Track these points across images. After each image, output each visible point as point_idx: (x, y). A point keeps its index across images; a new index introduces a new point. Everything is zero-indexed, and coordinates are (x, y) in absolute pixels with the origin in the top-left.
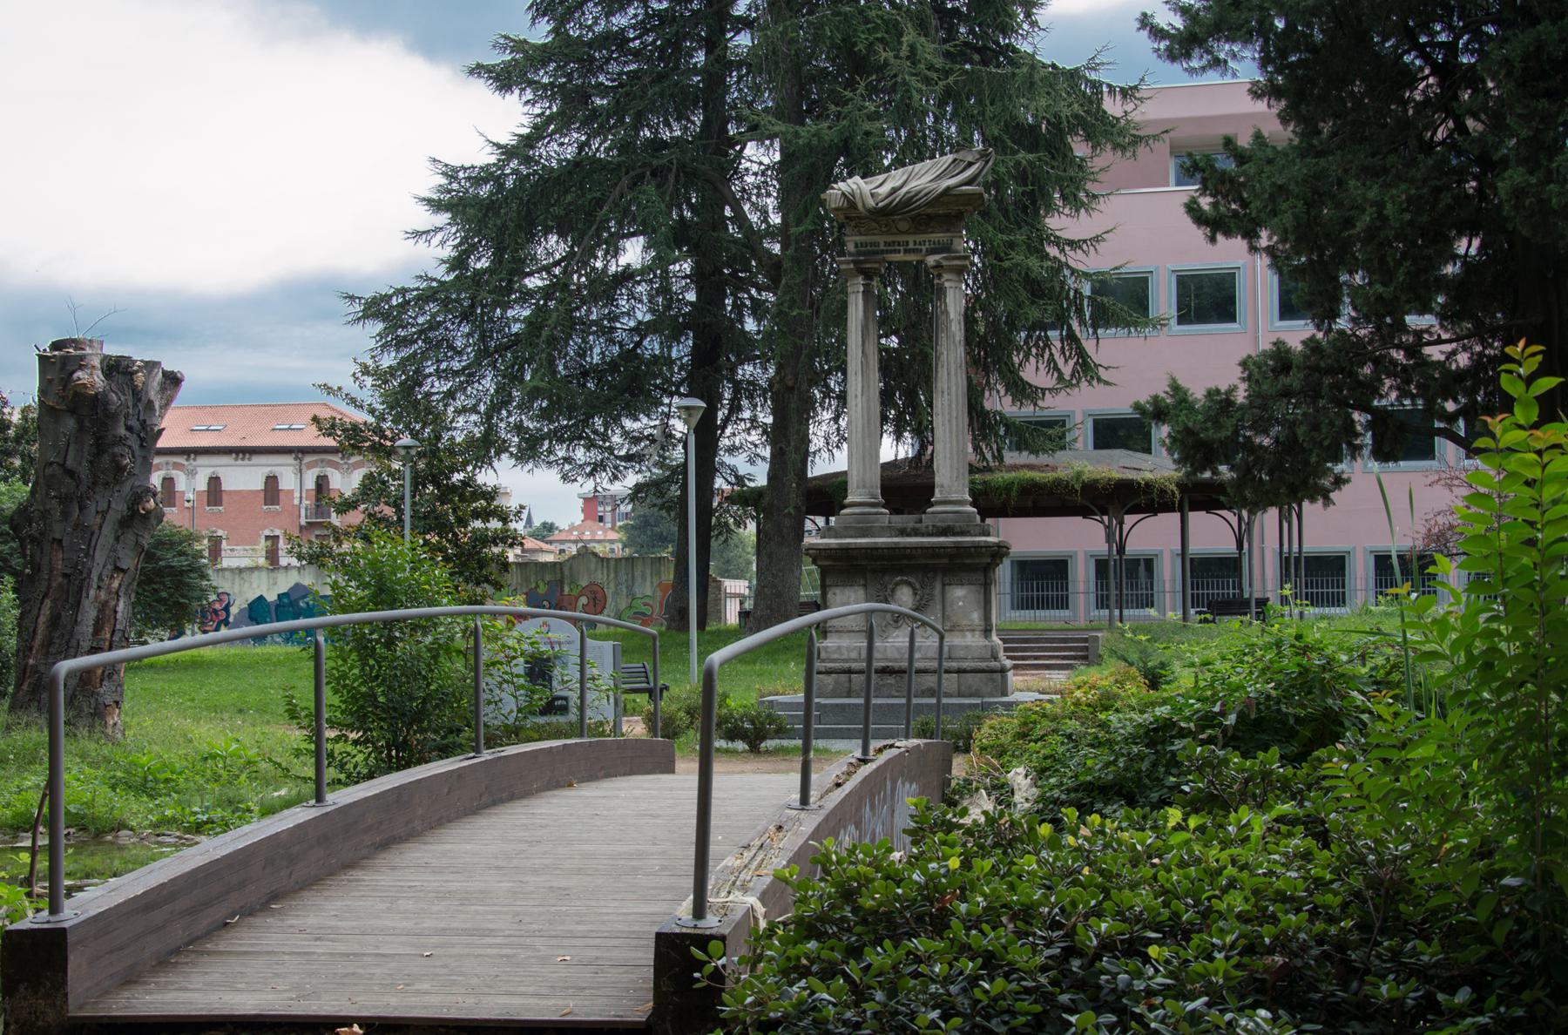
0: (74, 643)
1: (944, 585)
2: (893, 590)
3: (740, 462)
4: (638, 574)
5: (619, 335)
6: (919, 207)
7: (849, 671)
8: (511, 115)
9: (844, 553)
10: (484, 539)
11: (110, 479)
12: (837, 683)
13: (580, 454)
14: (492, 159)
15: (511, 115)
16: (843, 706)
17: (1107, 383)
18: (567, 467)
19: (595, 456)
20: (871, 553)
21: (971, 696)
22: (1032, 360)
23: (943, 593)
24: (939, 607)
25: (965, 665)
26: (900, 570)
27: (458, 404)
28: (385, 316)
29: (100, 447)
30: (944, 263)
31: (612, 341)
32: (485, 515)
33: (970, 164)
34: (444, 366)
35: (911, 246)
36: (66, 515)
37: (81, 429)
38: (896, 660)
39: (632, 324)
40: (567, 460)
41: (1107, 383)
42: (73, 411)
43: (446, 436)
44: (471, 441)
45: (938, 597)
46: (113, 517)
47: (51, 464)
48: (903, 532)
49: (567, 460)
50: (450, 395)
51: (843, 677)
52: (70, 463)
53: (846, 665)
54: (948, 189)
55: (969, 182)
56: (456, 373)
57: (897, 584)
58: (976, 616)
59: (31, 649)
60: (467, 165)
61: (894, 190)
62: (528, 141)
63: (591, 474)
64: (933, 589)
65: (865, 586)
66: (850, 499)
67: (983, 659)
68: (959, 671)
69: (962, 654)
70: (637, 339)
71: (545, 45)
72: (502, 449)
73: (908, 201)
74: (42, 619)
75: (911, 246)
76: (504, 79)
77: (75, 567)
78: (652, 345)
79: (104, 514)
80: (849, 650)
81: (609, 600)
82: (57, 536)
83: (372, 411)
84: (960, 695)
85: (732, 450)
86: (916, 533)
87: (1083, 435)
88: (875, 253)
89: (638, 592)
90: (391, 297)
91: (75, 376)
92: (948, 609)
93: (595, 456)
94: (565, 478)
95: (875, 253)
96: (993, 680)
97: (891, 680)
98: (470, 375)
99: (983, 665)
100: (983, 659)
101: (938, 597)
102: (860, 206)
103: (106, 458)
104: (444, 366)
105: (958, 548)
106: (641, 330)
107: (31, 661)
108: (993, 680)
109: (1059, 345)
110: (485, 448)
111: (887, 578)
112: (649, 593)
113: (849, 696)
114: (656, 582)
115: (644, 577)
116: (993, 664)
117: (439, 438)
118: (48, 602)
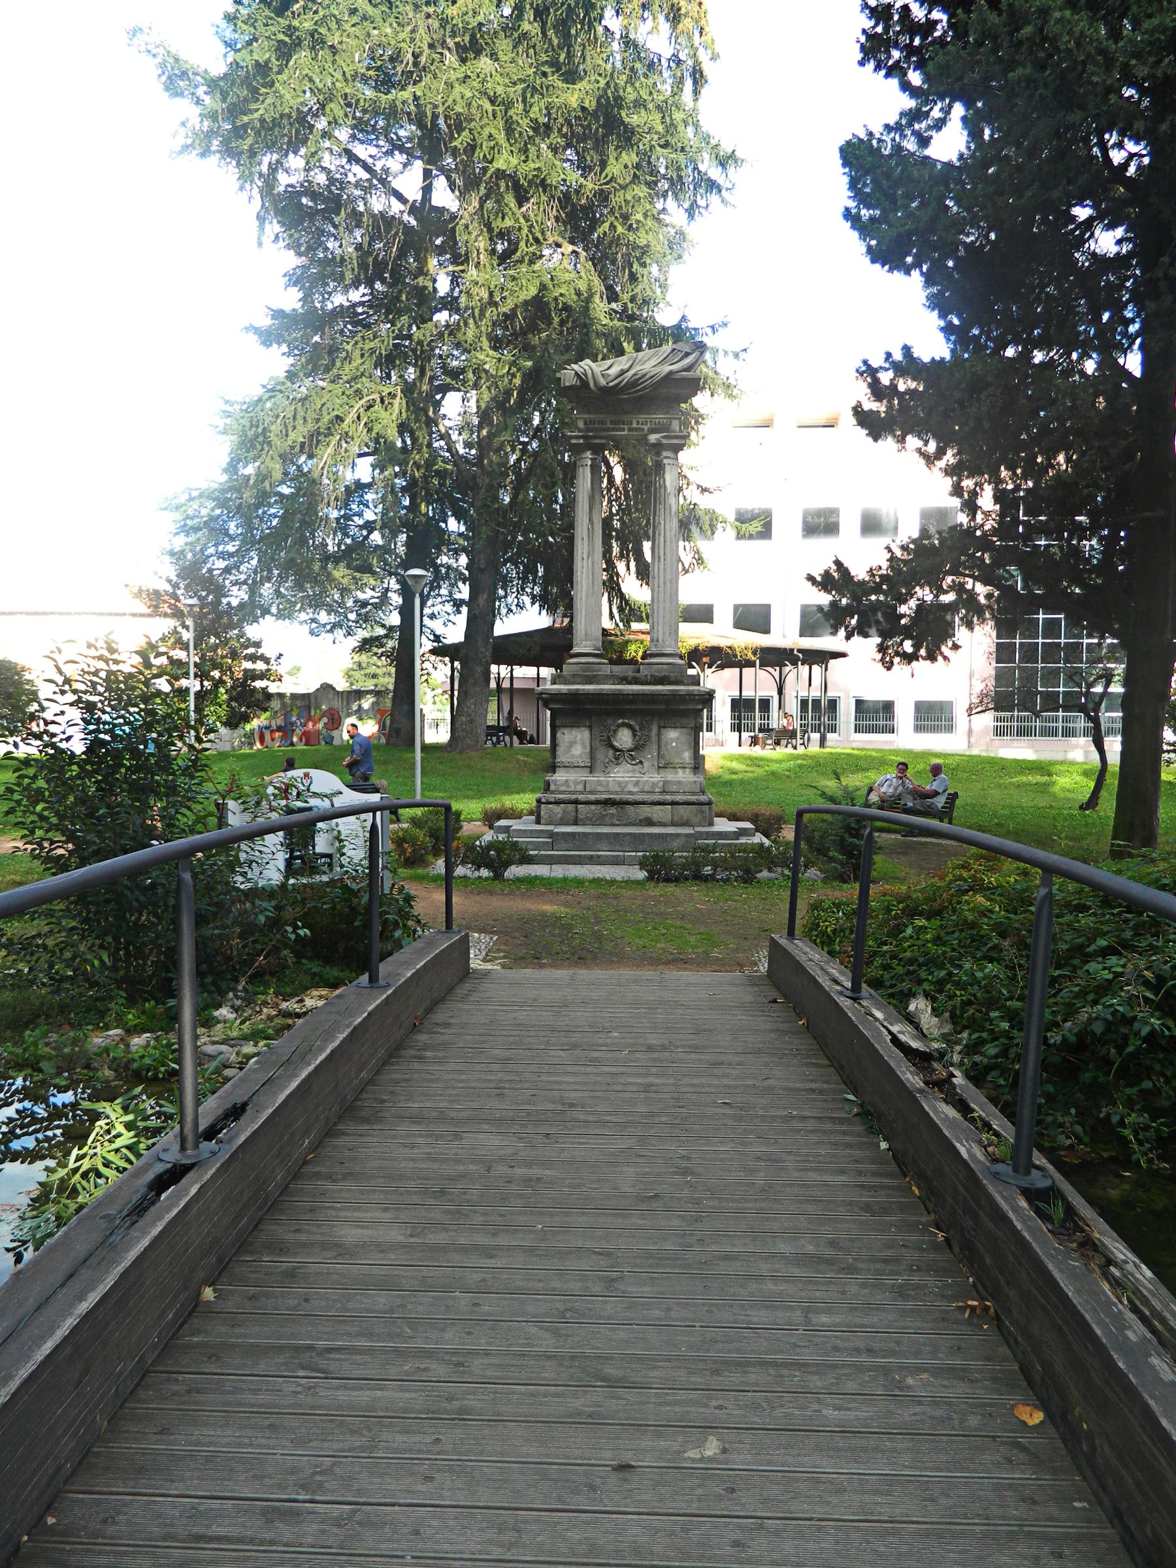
1: (660, 728)
2: (615, 731)
3: (437, 626)
5: (353, 531)
7: (576, 802)
9: (574, 697)
10: (253, 675)
12: (565, 812)
13: (323, 617)
16: (573, 835)
18: (314, 625)
19: (333, 618)
21: (682, 825)
23: (659, 735)
24: (655, 747)
25: (678, 798)
26: (622, 714)
27: (232, 578)
30: (664, 441)
31: (346, 535)
32: (253, 658)
33: (687, 354)
34: (221, 548)
35: (634, 425)
38: (617, 793)
39: (361, 522)
40: (313, 620)
43: (225, 601)
44: (242, 605)
45: (654, 738)
48: (624, 680)
49: (313, 620)
50: (227, 570)
51: (571, 807)
53: (573, 797)
54: (671, 373)
56: (231, 555)
57: (619, 726)
58: (687, 756)
61: (623, 372)
63: (331, 631)
64: (650, 730)
65: (590, 728)
66: (576, 650)
67: (694, 793)
68: (673, 803)
69: (674, 788)
70: (365, 533)
72: (266, 611)
73: (635, 383)
75: (634, 425)
76: (268, 338)
78: (376, 538)
80: (576, 783)
83: (169, 581)
84: (673, 824)
85: (432, 616)
86: (636, 681)
87: (724, 617)
88: (601, 430)
93: (333, 618)
94: (312, 633)
95: (601, 430)
97: (613, 810)
98: (240, 555)
99: (694, 798)
101: (654, 738)
102: (592, 384)
104: (221, 548)
105: (674, 696)
106: (369, 526)
108: (702, 812)
110: (252, 610)
111: (609, 721)
113: (575, 823)
116: (703, 798)
117: (220, 603)
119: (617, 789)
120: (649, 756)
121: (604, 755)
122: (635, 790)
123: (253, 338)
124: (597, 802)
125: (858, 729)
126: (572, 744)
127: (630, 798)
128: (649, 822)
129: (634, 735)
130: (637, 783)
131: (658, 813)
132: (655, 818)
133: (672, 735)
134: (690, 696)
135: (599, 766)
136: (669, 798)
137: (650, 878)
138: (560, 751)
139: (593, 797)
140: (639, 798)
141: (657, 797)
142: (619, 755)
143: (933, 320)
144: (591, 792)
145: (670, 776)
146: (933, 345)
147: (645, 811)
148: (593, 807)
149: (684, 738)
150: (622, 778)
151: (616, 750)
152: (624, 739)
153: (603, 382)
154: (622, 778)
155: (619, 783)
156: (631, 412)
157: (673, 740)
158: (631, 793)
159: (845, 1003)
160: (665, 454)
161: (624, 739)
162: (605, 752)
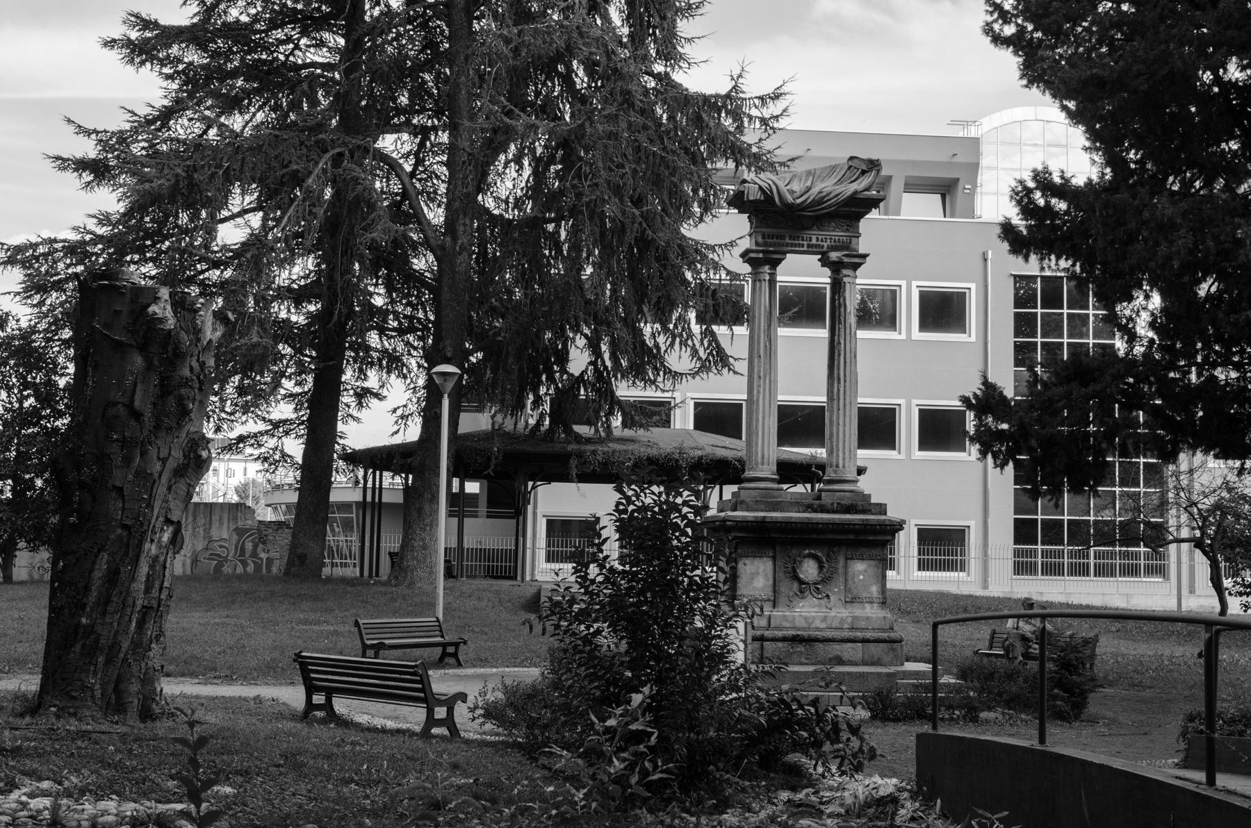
0: (130, 600)
1: (847, 559)
4: (215, 518)
6: (830, 206)
8: (149, 88)
11: (174, 425)
14: (127, 126)
15: (149, 88)
17: (735, 373)
20: (786, 526)
21: (873, 664)
22: (677, 346)
23: (846, 567)
25: (869, 635)
28: (25, 264)
29: (165, 389)
30: (846, 260)
35: (814, 241)
36: (128, 461)
37: (149, 367)
38: (803, 629)
41: (735, 373)
42: (143, 349)
45: (841, 570)
46: (171, 464)
47: (116, 404)
52: (137, 404)
54: (856, 192)
55: (868, 189)
58: (875, 590)
59: (83, 607)
60: (100, 129)
62: (166, 115)
64: (837, 562)
65: (774, 559)
67: (883, 630)
68: (865, 641)
69: (863, 624)
71: (194, 25)
74: (97, 574)
75: (814, 241)
77: (137, 519)
79: (164, 461)
81: (187, 541)
82: (118, 484)
84: (865, 663)
87: (683, 419)
89: (215, 533)
90: (37, 245)
91: (151, 309)
92: (850, 582)
96: (894, 650)
97: (801, 648)
99: (885, 635)
100: (883, 630)
102: (777, 200)
103: (171, 403)
107: (84, 620)
109: (699, 337)
111: (794, 552)
112: (225, 536)
114: (233, 527)
115: (221, 524)
118: (105, 556)
119: (804, 625)
120: (836, 590)
121: (788, 588)
122: (823, 625)
123: (115, 55)
124: (784, 639)
125: (922, 566)
126: (754, 575)
127: (819, 634)
128: (840, 661)
129: (821, 567)
130: (824, 619)
131: (847, 651)
132: (846, 656)
133: (860, 568)
134: (867, 528)
135: (782, 600)
136: (859, 634)
137: (873, 718)
138: (742, 583)
139: (780, 634)
140: (829, 634)
141: (846, 634)
142: (804, 588)
143: (1078, 135)
144: (777, 628)
145: (858, 611)
146: (1079, 162)
147: (836, 649)
148: (780, 644)
149: (871, 571)
150: (807, 613)
151: (801, 582)
152: (809, 570)
153: (790, 199)
154: (807, 613)
155: (806, 618)
156: (810, 228)
157: (860, 572)
158: (818, 629)
159: (1209, 792)
160: (845, 272)
161: (809, 570)
162: (791, 583)
